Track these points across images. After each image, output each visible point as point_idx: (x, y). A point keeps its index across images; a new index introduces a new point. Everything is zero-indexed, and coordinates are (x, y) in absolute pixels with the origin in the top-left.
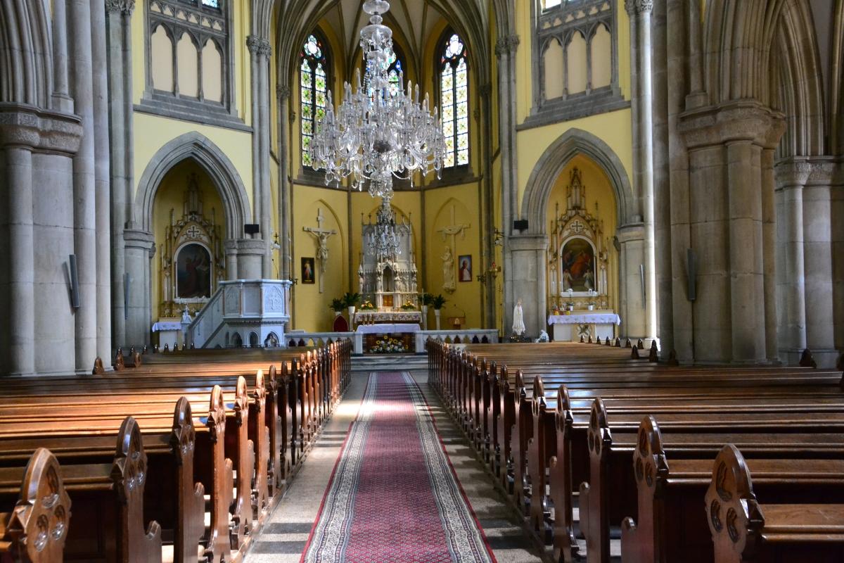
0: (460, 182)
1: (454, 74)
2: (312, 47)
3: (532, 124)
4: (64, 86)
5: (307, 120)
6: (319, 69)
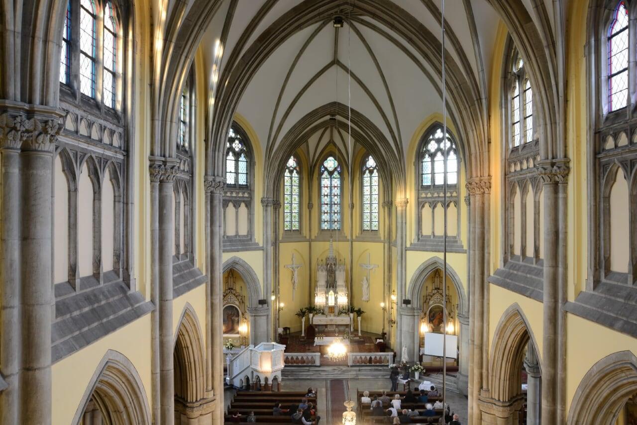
1: (371, 177)
3: (414, 248)
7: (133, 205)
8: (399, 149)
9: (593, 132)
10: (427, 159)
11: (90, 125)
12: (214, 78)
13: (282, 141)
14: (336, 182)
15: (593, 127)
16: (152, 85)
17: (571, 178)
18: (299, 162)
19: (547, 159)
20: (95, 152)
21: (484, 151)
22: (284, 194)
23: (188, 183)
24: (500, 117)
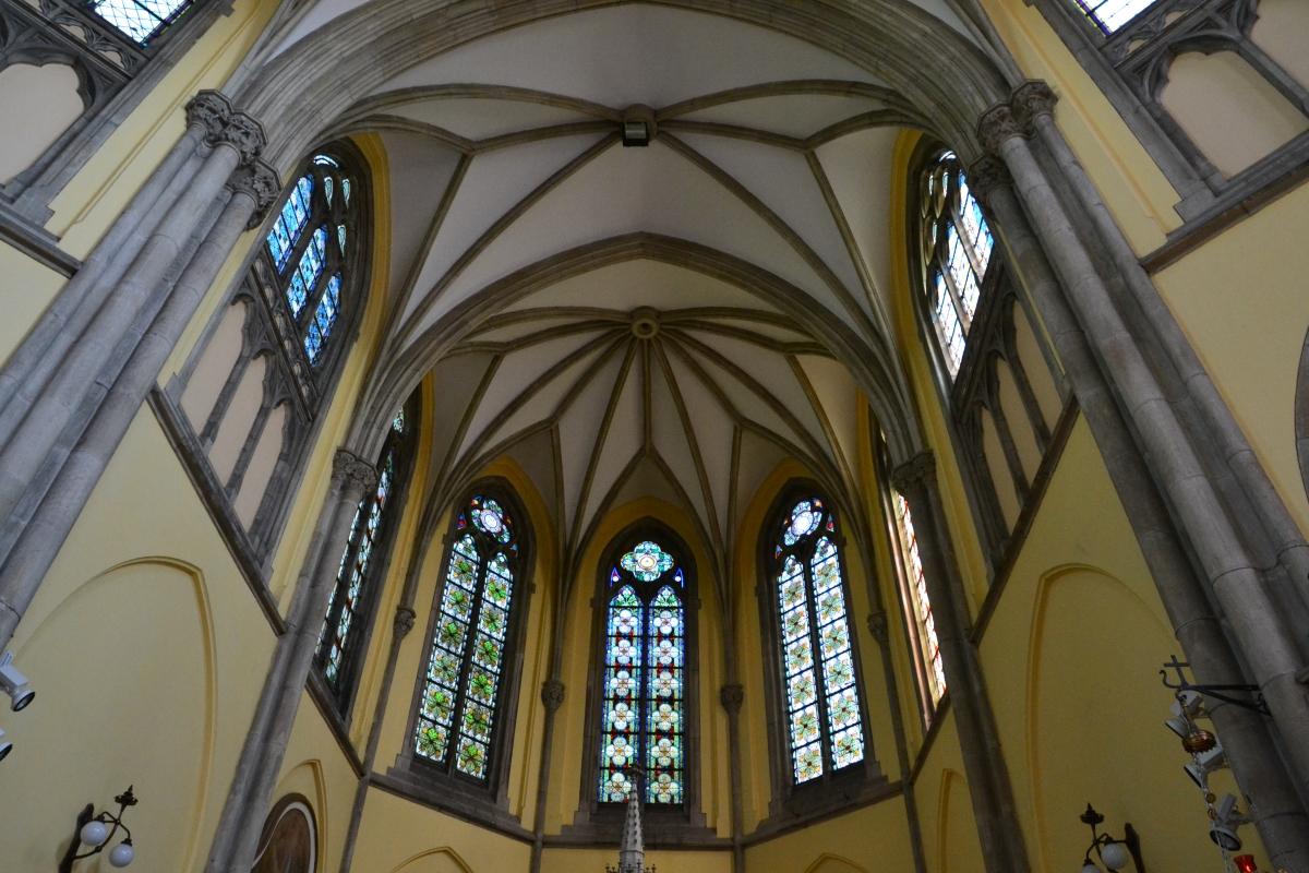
0: (849, 805)
1: (808, 574)
2: (491, 521)
5: (448, 651)
6: (500, 564)
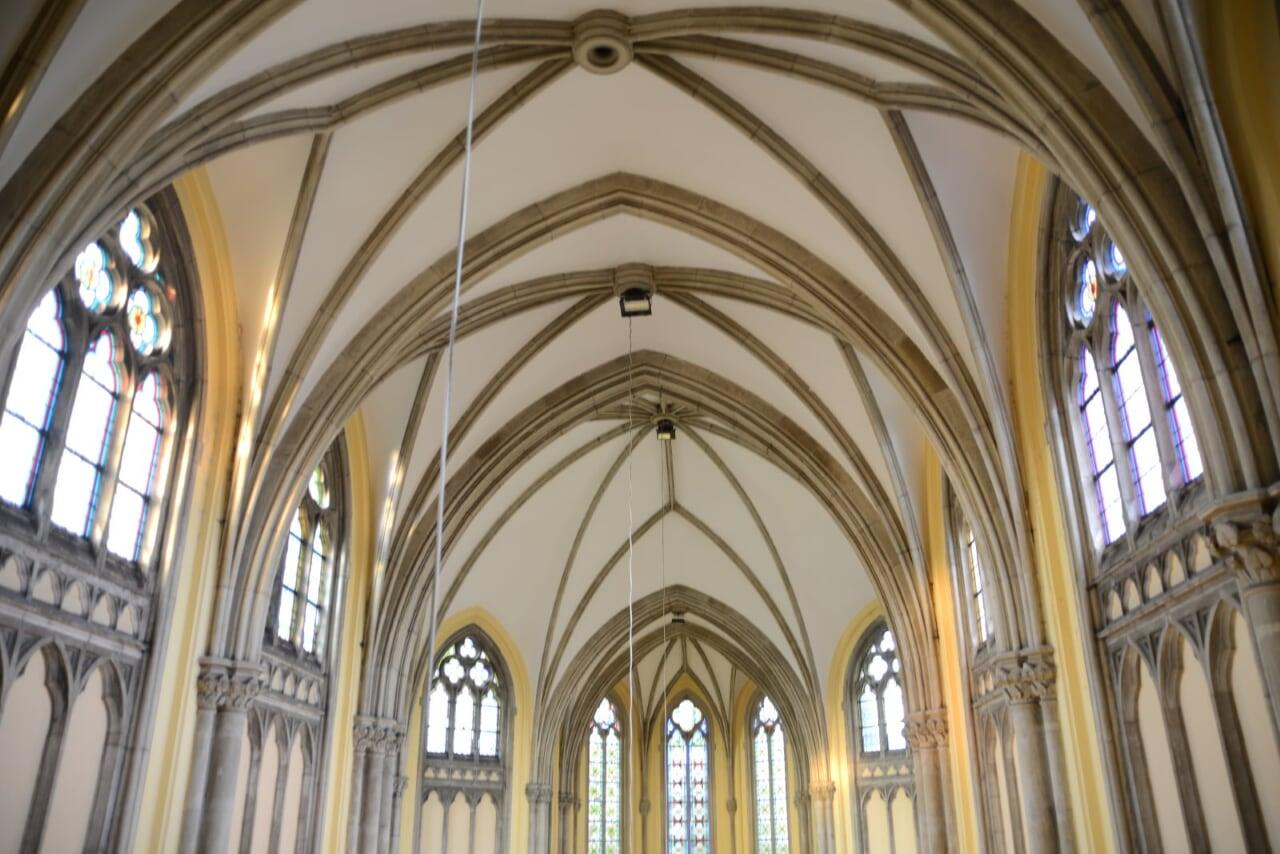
1: (769, 741)
4: (1233, 225)
7: (146, 753)
8: (806, 668)
9: (1083, 586)
10: (868, 697)
11: (63, 584)
12: (387, 523)
13: (571, 665)
14: (699, 753)
15: (1082, 577)
16: (224, 522)
17: (1061, 686)
18: (621, 714)
19: (1011, 649)
20: (63, 637)
21: (927, 654)
22: (588, 781)
23: (314, 730)
24: (949, 582)
